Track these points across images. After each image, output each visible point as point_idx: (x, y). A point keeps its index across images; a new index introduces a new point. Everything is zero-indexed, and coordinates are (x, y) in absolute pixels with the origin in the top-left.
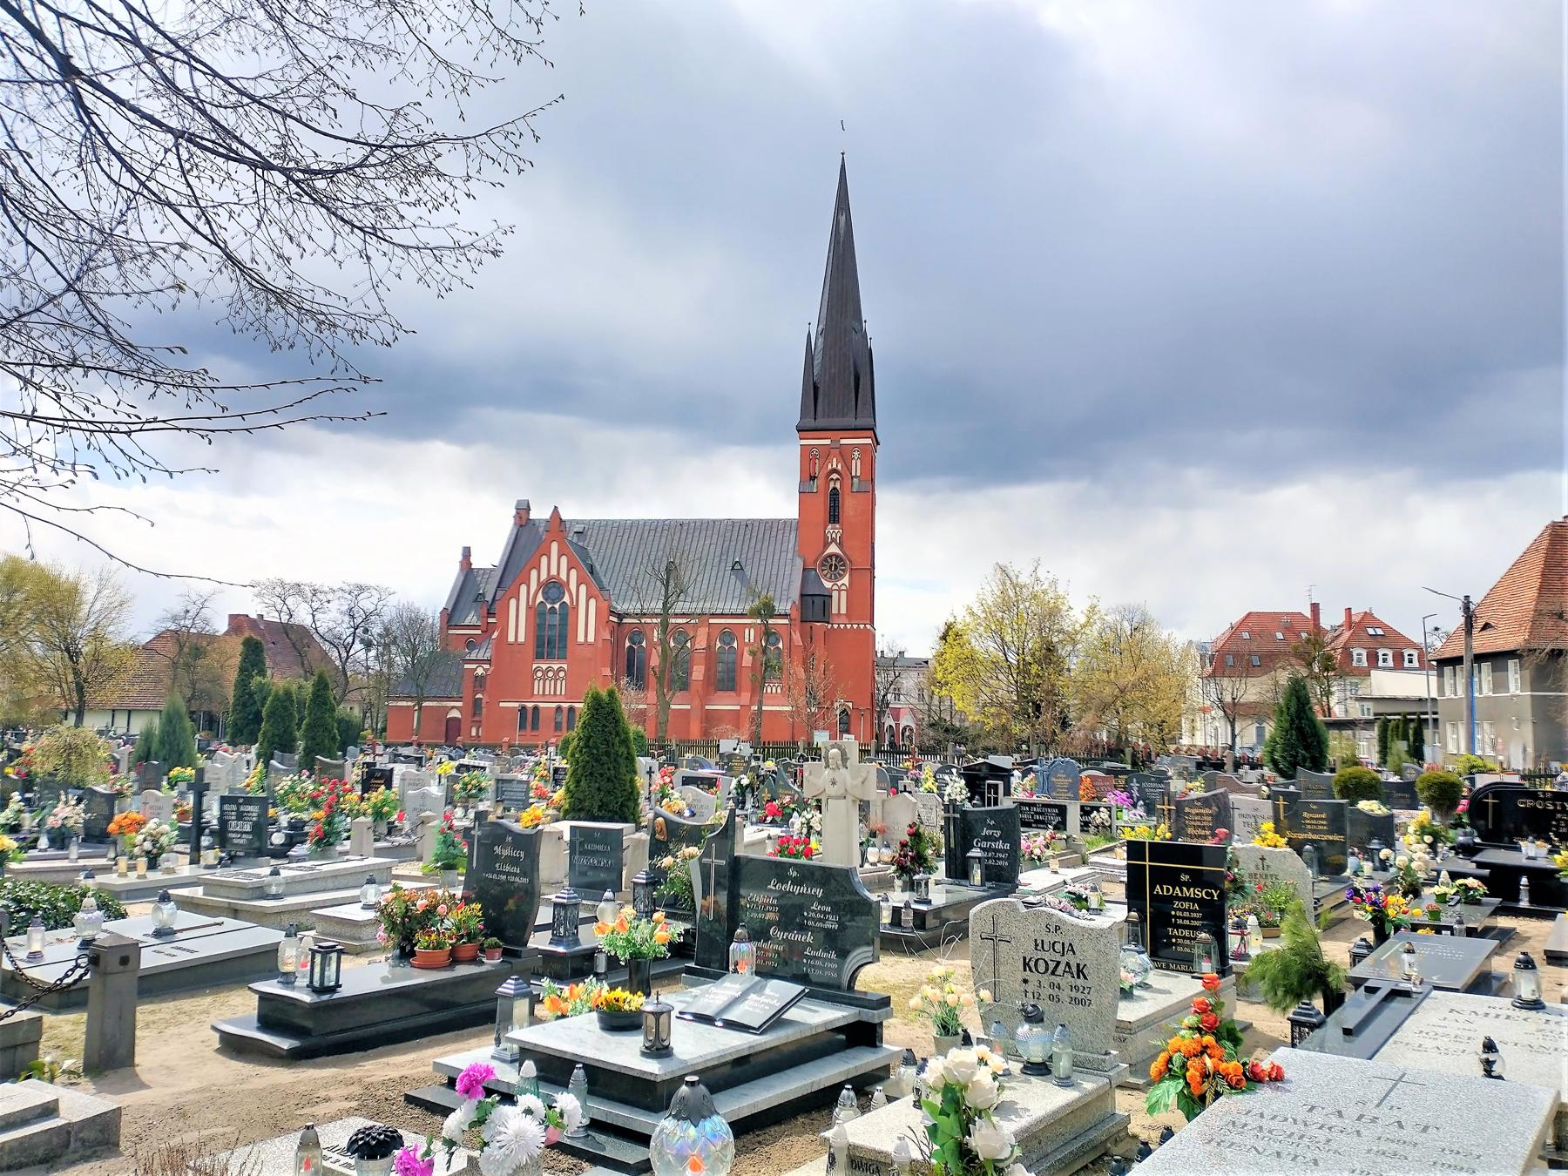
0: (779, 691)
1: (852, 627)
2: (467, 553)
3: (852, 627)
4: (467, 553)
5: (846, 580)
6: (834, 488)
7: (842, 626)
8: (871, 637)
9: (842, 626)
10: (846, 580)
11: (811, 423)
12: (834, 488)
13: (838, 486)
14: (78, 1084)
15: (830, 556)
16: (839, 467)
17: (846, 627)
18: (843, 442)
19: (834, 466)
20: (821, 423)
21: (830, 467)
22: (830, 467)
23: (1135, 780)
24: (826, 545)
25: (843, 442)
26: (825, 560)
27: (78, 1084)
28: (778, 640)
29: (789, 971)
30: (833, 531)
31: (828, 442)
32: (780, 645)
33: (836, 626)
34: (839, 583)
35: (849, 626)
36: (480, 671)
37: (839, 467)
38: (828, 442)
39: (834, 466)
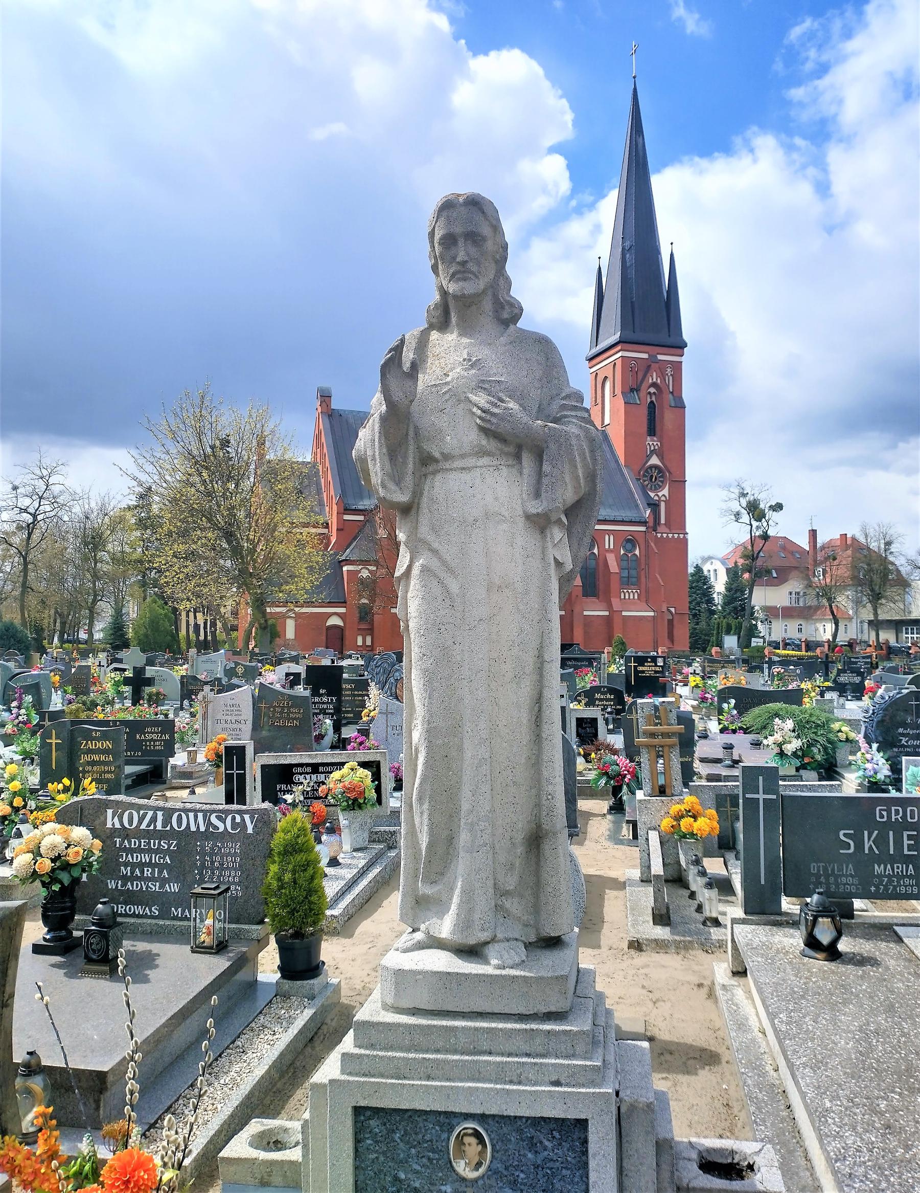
0: (636, 597)
1: (673, 537)
2: (325, 397)
3: (673, 537)
4: (325, 397)
5: (665, 491)
6: (652, 402)
7: (665, 535)
8: (683, 544)
9: (665, 535)
10: (665, 491)
11: (631, 336)
12: (652, 402)
13: (654, 399)
14: (871, 961)
15: (651, 467)
16: (659, 381)
17: (667, 536)
18: (660, 357)
19: (655, 380)
20: (638, 336)
21: (650, 381)
22: (650, 381)
23: (733, 701)
24: (649, 457)
25: (660, 357)
26: (646, 471)
27: (871, 961)
28: (634, 547)
29: (410, 1113)
30: (652, 443)
31: (645, 356)
32: (637, 552)
33: (659, 535)
34: (660, 494)
35: (670, 536)
36: (365, 574)
37: (659, 381)
38: (645, 356)
39: (655, 380)
